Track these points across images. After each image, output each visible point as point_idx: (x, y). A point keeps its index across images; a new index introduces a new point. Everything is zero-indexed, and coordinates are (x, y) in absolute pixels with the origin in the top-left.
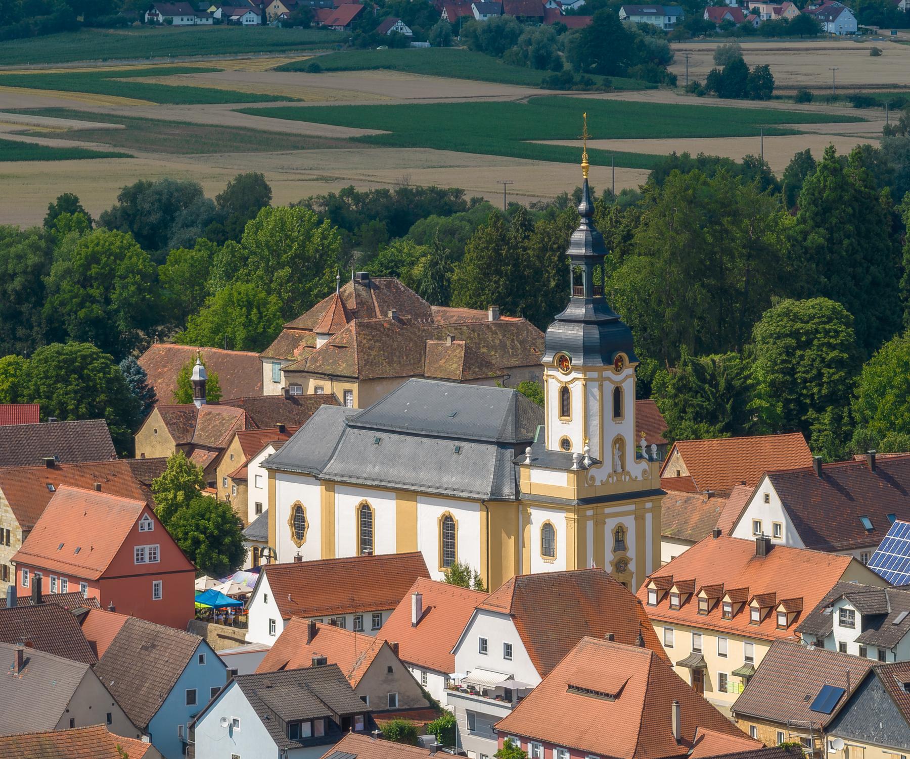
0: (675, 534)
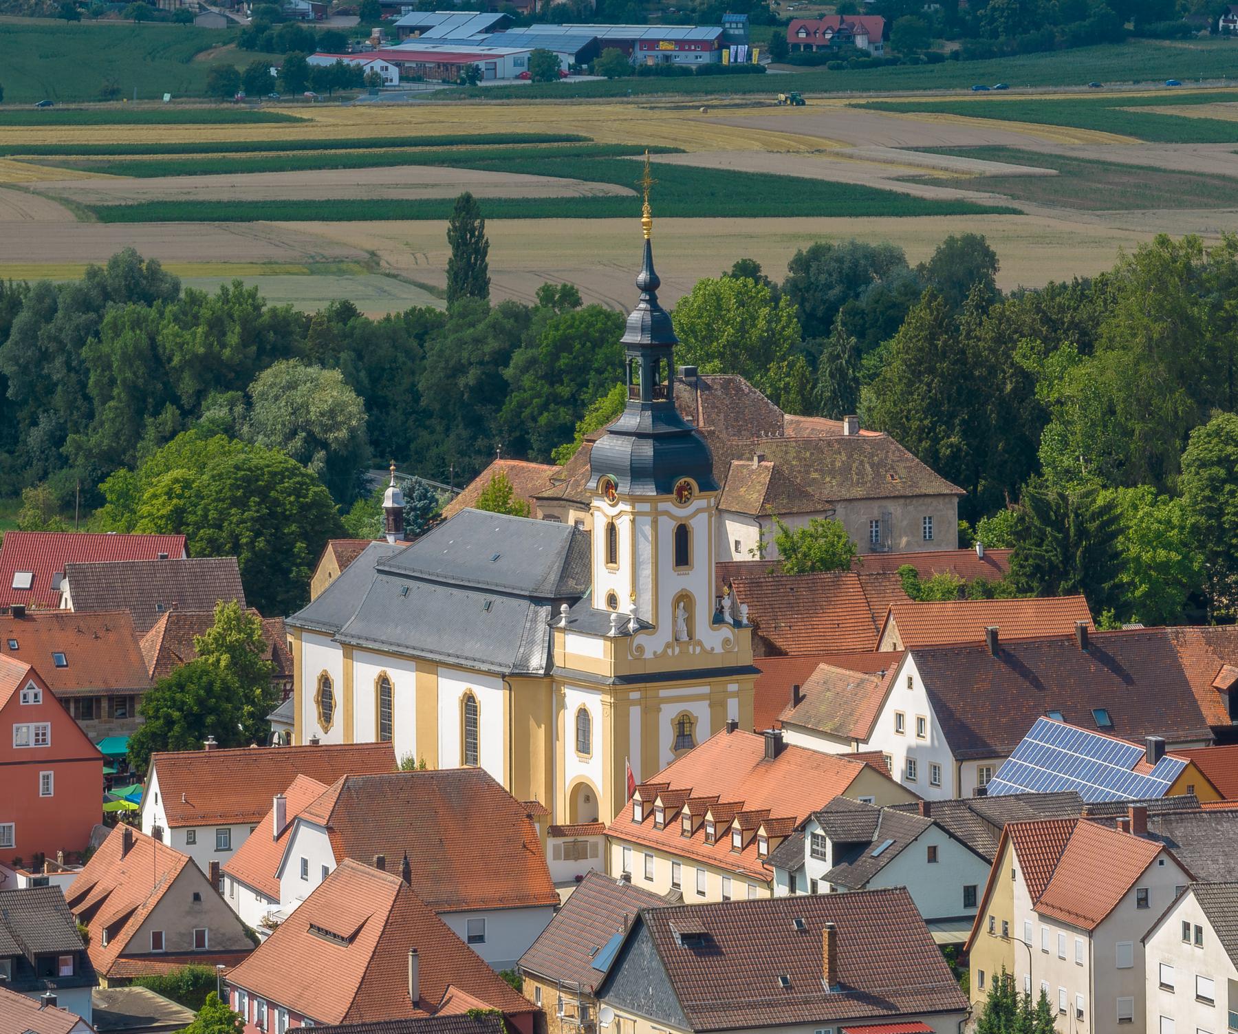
0: (836, 730)
